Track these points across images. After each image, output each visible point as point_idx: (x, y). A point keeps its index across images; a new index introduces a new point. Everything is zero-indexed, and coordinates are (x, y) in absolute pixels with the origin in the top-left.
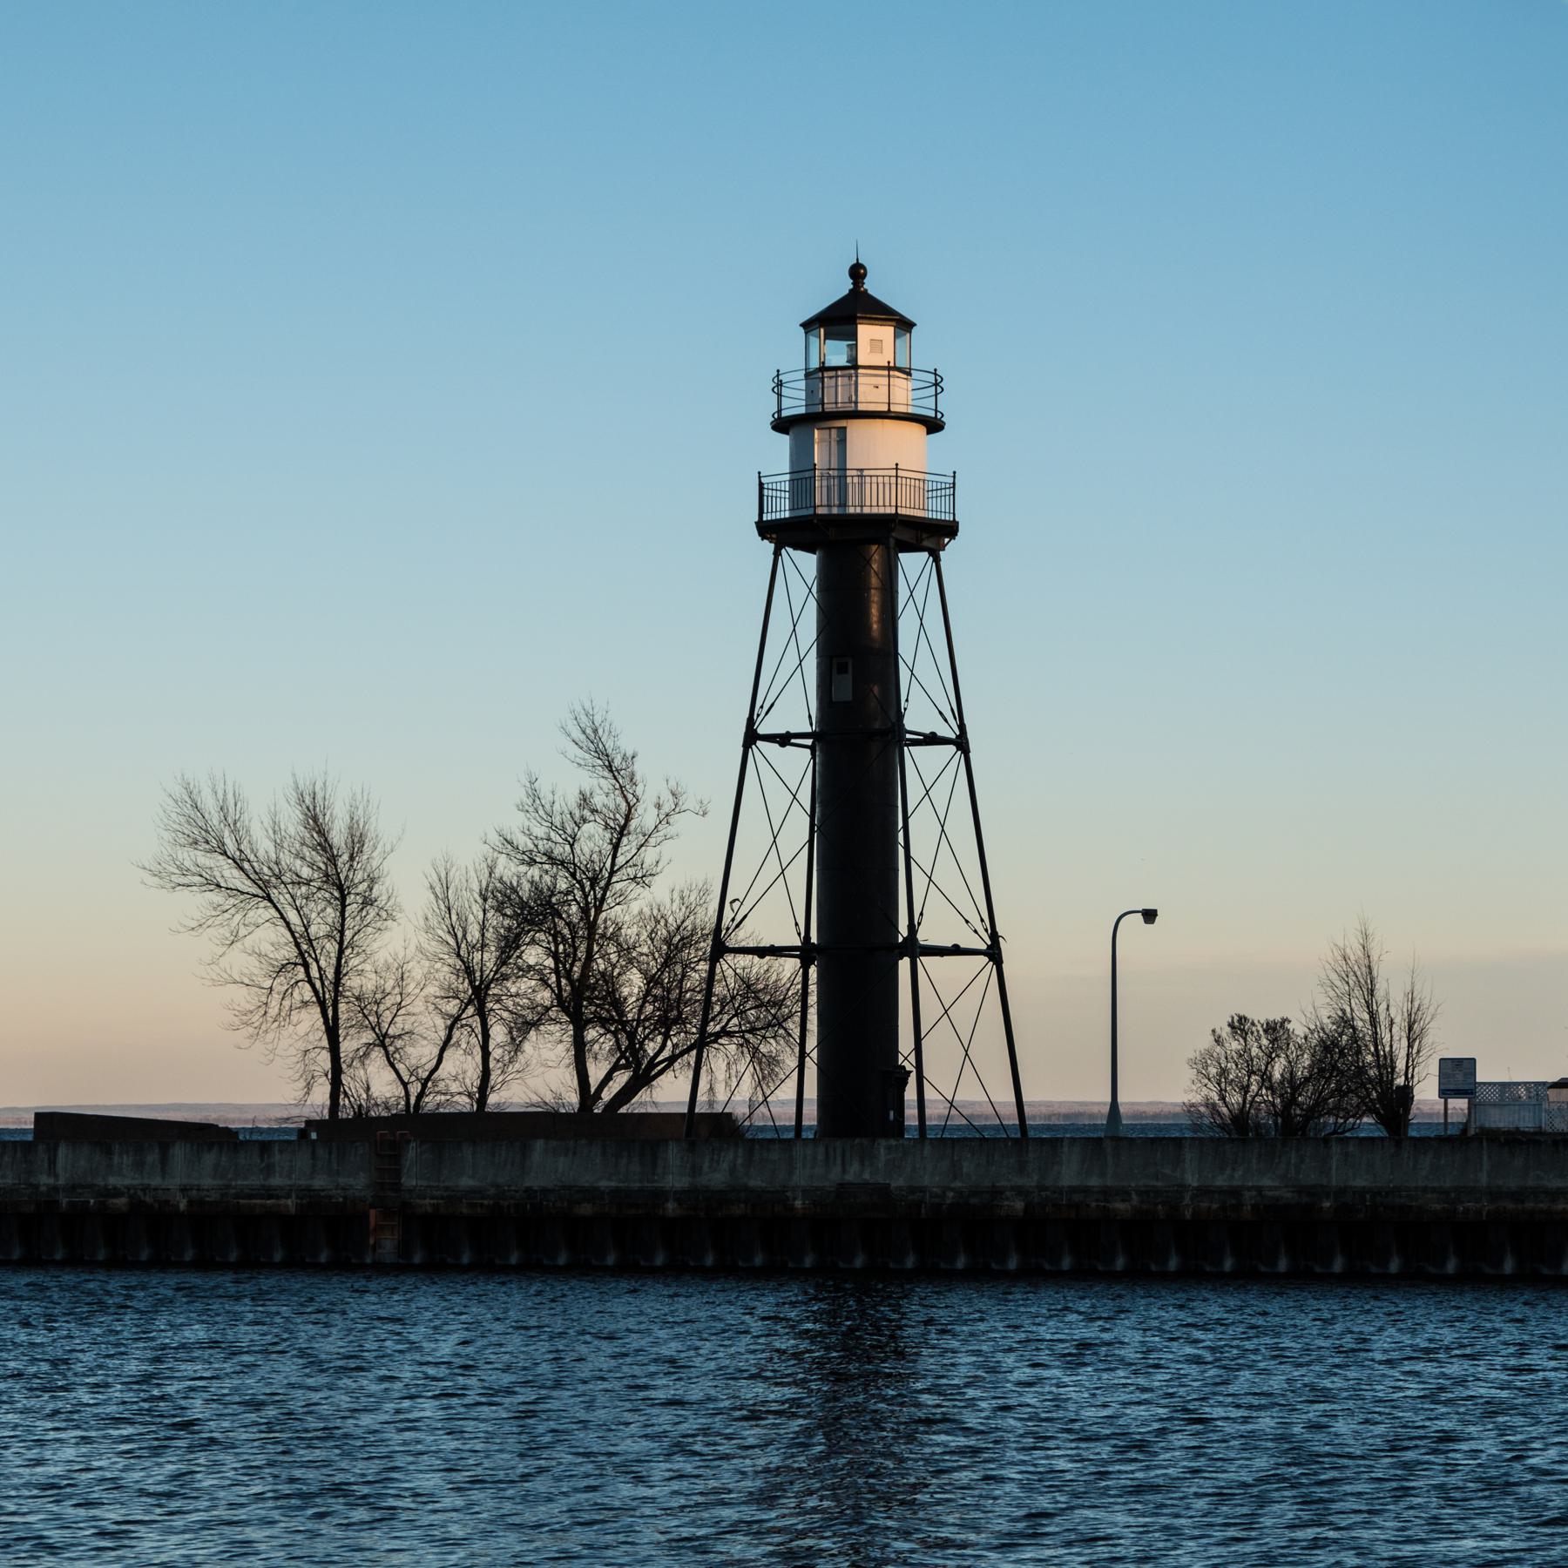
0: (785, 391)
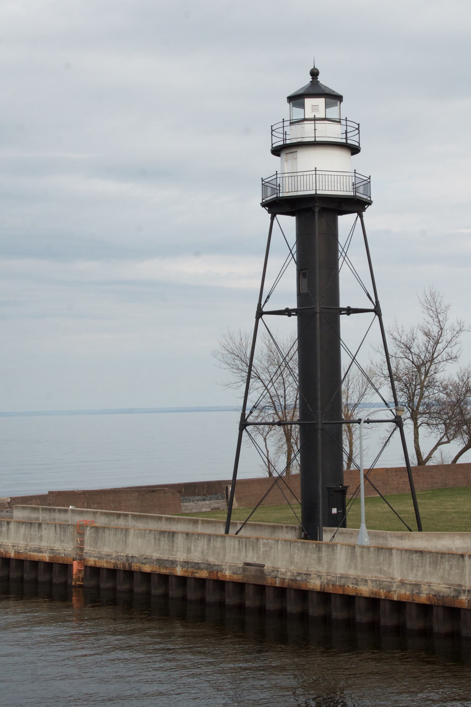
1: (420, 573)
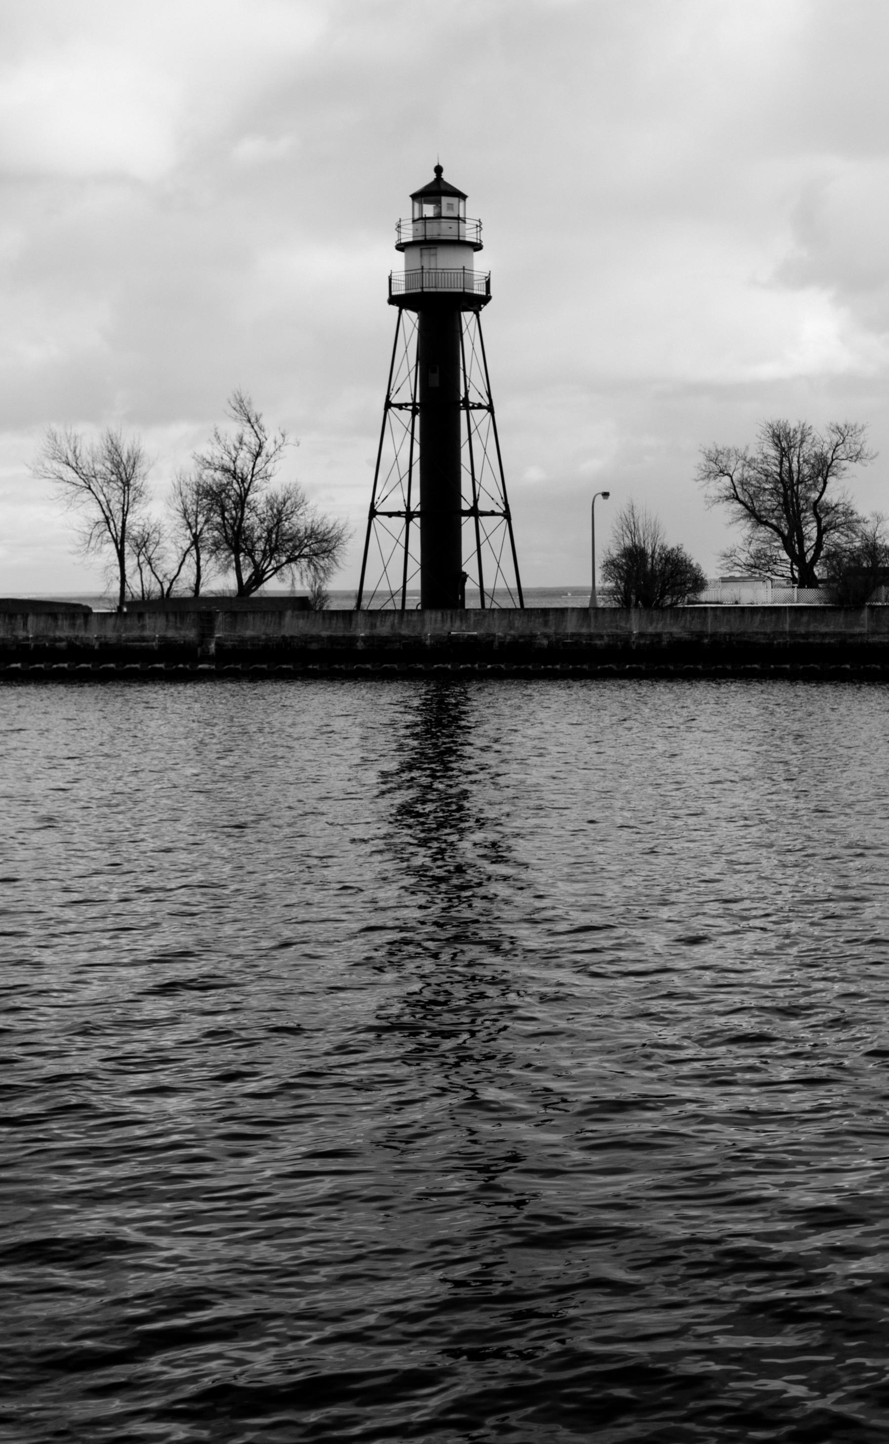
0: (402, 230)
1: (660, 625)
